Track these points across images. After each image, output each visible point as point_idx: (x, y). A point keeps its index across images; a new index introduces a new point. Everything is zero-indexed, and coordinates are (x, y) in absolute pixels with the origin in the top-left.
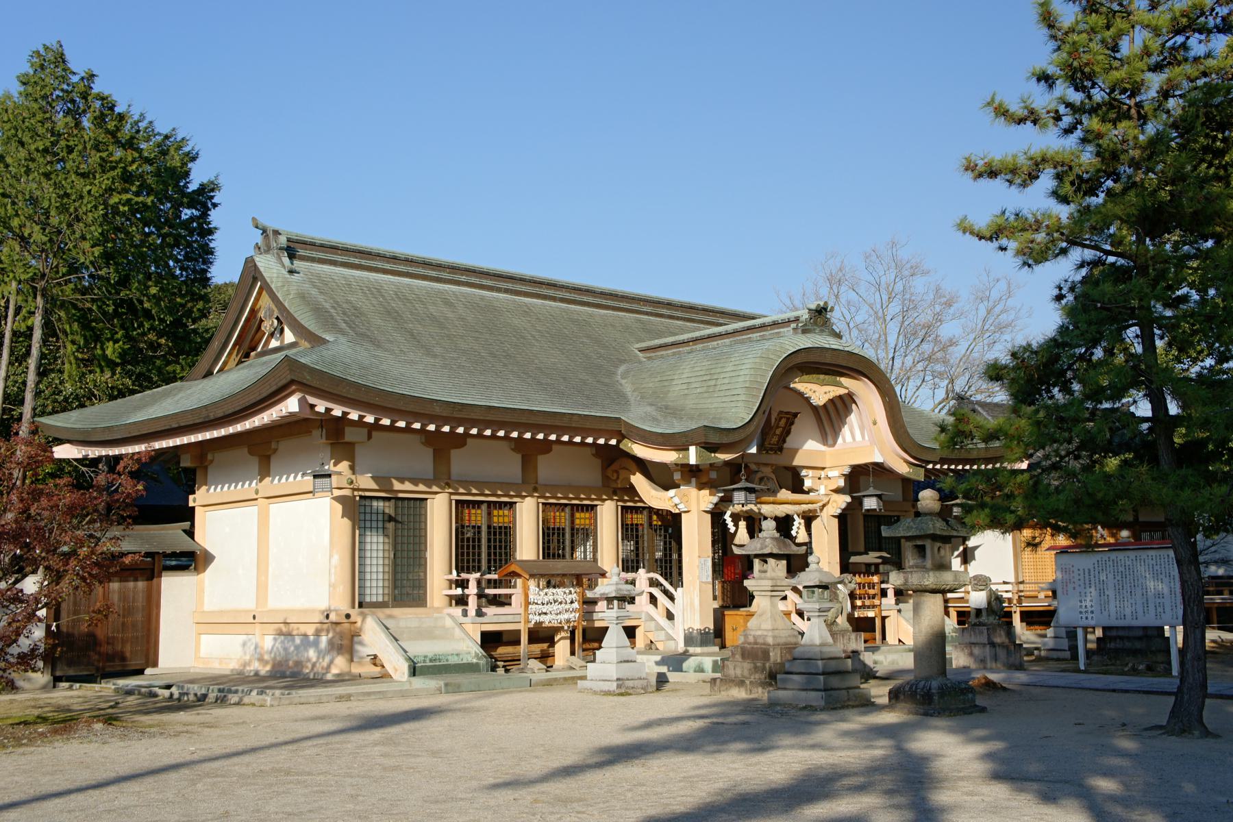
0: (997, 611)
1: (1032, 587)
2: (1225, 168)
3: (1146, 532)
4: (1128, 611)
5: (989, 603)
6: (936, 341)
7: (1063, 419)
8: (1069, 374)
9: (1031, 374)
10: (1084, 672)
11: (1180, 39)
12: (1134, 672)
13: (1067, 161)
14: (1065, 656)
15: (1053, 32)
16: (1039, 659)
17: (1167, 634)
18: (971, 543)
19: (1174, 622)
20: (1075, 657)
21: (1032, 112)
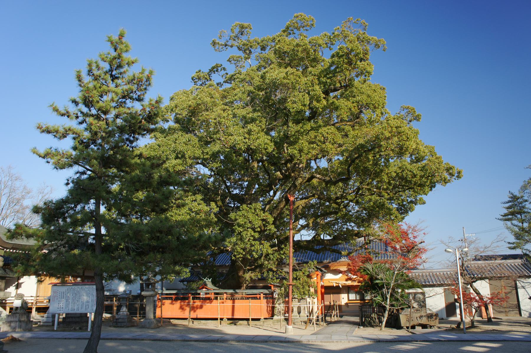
0: (26, 309)
1: (42, 298)
2: (132, 147)
3: (86, 279)
4: (76, 308)
5: (22, 304)
6: (21, 205)
7: (61, 231)
8: (66, 215)
9: (51, 213)
10: (56, 331)
11: (124, 100)
12: (75, 330)
13: (78, 132)
14: (48, 326)
15: (80, 83)
16: (40, 326)
17: (88, 316)
18: (20, 281)
19: (91, 311)
20: (53, 325)
21: (68, 112)
